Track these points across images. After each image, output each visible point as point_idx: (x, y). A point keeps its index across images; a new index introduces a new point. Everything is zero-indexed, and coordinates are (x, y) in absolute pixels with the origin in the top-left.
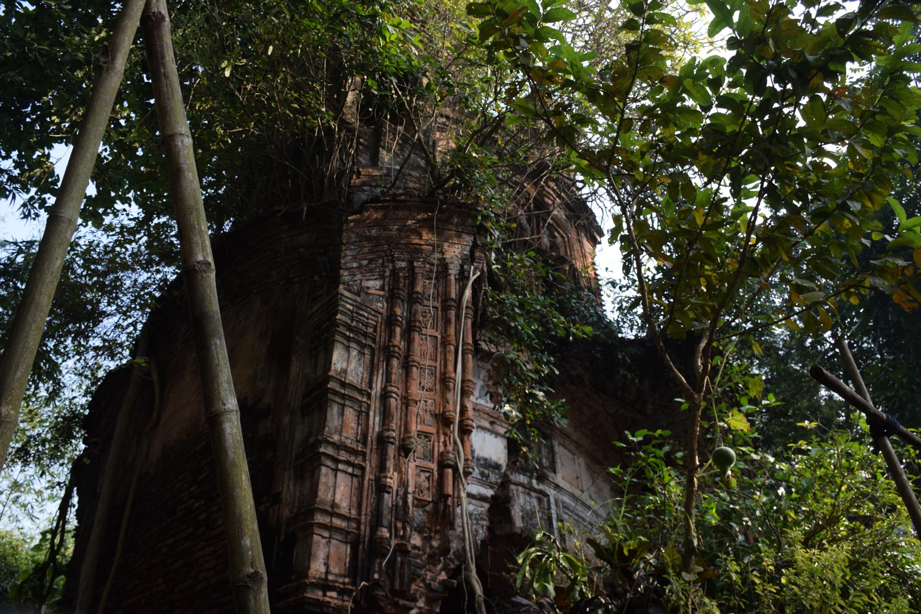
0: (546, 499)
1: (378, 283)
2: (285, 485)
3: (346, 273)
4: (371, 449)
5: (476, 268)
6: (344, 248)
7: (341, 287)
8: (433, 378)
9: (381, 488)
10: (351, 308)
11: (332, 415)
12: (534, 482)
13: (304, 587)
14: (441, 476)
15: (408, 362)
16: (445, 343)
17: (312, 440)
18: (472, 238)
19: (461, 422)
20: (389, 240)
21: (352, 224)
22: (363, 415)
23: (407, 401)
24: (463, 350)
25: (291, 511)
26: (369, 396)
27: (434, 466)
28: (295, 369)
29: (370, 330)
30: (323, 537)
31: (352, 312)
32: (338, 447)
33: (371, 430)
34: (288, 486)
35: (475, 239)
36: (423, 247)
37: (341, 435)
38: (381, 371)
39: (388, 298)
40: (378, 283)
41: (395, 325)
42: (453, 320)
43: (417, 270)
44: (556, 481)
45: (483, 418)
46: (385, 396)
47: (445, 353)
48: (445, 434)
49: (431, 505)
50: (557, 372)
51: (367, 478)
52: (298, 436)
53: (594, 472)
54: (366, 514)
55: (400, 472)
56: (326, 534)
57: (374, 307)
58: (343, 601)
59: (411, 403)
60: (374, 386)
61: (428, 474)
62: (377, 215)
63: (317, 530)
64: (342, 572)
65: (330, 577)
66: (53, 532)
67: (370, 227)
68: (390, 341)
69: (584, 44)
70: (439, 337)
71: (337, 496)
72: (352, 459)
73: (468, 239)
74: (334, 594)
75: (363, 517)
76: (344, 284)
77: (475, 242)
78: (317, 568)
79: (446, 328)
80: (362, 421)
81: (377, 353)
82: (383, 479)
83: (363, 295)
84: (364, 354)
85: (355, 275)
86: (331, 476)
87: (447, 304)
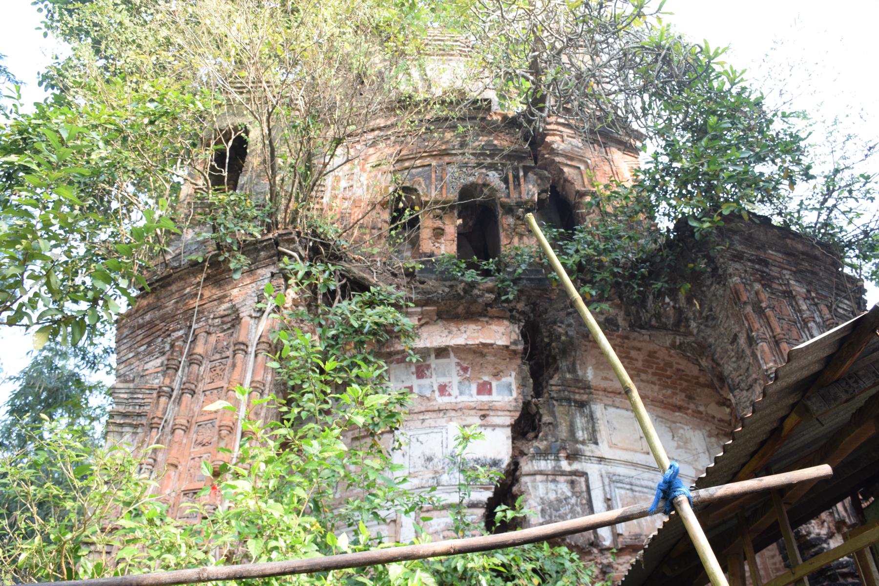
0: (583, 479)
10: (126, 396)
45: (469, 415)
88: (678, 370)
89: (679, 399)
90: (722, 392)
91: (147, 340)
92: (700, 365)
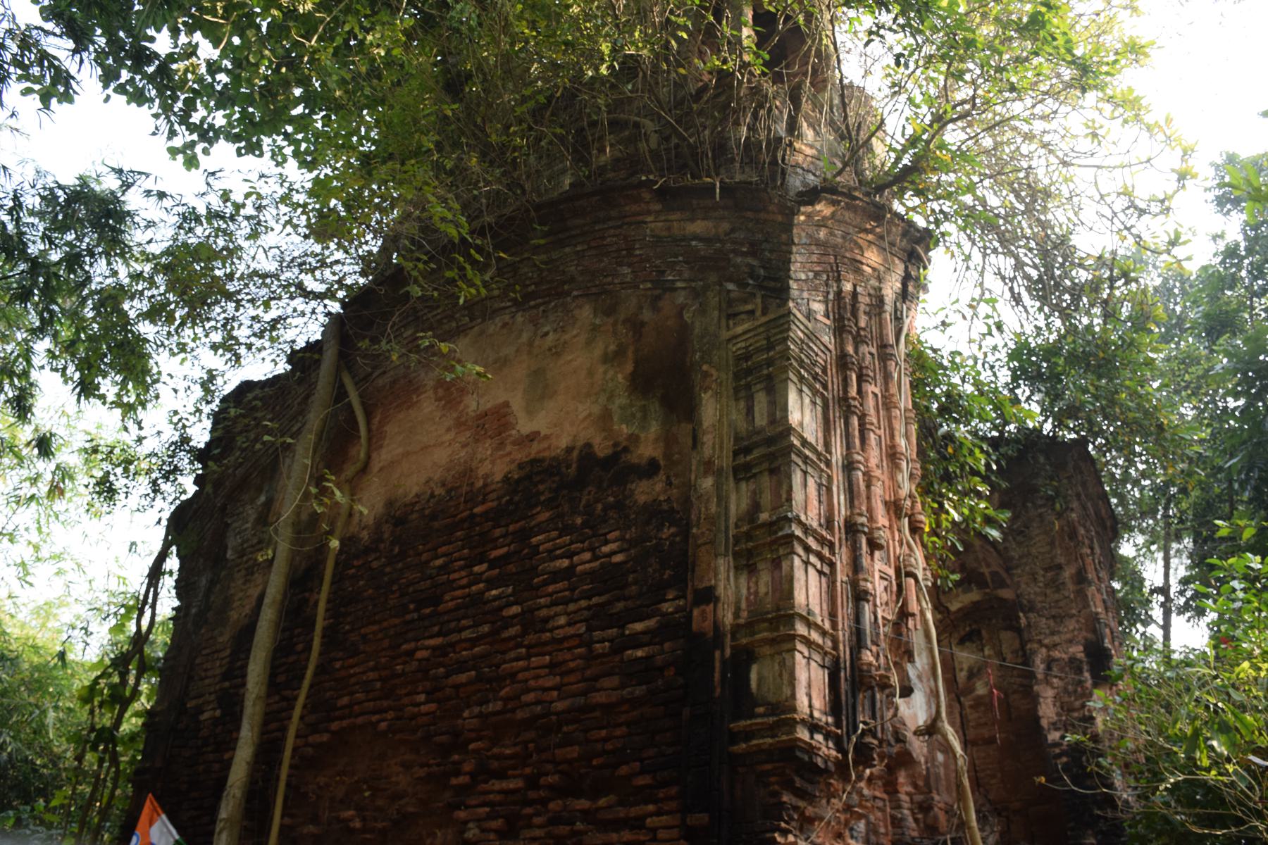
2: (722, 576)
4: (840, 539)
6: (794, 249)
13: (793, 723)
17: (764, 516)
21: (802, 218)
22: (825, 489)
25: (736, 615)
26: (828, 464)
28: (709, 410)
31: (803, 342)
35: (906, 268)
36: (865, 268)
38: (838, 432)
41: (851, 369)
46: (849, 467)
61: (886, 583)
80: (824, 498)
82: (862, 583)
91: (818, 269)
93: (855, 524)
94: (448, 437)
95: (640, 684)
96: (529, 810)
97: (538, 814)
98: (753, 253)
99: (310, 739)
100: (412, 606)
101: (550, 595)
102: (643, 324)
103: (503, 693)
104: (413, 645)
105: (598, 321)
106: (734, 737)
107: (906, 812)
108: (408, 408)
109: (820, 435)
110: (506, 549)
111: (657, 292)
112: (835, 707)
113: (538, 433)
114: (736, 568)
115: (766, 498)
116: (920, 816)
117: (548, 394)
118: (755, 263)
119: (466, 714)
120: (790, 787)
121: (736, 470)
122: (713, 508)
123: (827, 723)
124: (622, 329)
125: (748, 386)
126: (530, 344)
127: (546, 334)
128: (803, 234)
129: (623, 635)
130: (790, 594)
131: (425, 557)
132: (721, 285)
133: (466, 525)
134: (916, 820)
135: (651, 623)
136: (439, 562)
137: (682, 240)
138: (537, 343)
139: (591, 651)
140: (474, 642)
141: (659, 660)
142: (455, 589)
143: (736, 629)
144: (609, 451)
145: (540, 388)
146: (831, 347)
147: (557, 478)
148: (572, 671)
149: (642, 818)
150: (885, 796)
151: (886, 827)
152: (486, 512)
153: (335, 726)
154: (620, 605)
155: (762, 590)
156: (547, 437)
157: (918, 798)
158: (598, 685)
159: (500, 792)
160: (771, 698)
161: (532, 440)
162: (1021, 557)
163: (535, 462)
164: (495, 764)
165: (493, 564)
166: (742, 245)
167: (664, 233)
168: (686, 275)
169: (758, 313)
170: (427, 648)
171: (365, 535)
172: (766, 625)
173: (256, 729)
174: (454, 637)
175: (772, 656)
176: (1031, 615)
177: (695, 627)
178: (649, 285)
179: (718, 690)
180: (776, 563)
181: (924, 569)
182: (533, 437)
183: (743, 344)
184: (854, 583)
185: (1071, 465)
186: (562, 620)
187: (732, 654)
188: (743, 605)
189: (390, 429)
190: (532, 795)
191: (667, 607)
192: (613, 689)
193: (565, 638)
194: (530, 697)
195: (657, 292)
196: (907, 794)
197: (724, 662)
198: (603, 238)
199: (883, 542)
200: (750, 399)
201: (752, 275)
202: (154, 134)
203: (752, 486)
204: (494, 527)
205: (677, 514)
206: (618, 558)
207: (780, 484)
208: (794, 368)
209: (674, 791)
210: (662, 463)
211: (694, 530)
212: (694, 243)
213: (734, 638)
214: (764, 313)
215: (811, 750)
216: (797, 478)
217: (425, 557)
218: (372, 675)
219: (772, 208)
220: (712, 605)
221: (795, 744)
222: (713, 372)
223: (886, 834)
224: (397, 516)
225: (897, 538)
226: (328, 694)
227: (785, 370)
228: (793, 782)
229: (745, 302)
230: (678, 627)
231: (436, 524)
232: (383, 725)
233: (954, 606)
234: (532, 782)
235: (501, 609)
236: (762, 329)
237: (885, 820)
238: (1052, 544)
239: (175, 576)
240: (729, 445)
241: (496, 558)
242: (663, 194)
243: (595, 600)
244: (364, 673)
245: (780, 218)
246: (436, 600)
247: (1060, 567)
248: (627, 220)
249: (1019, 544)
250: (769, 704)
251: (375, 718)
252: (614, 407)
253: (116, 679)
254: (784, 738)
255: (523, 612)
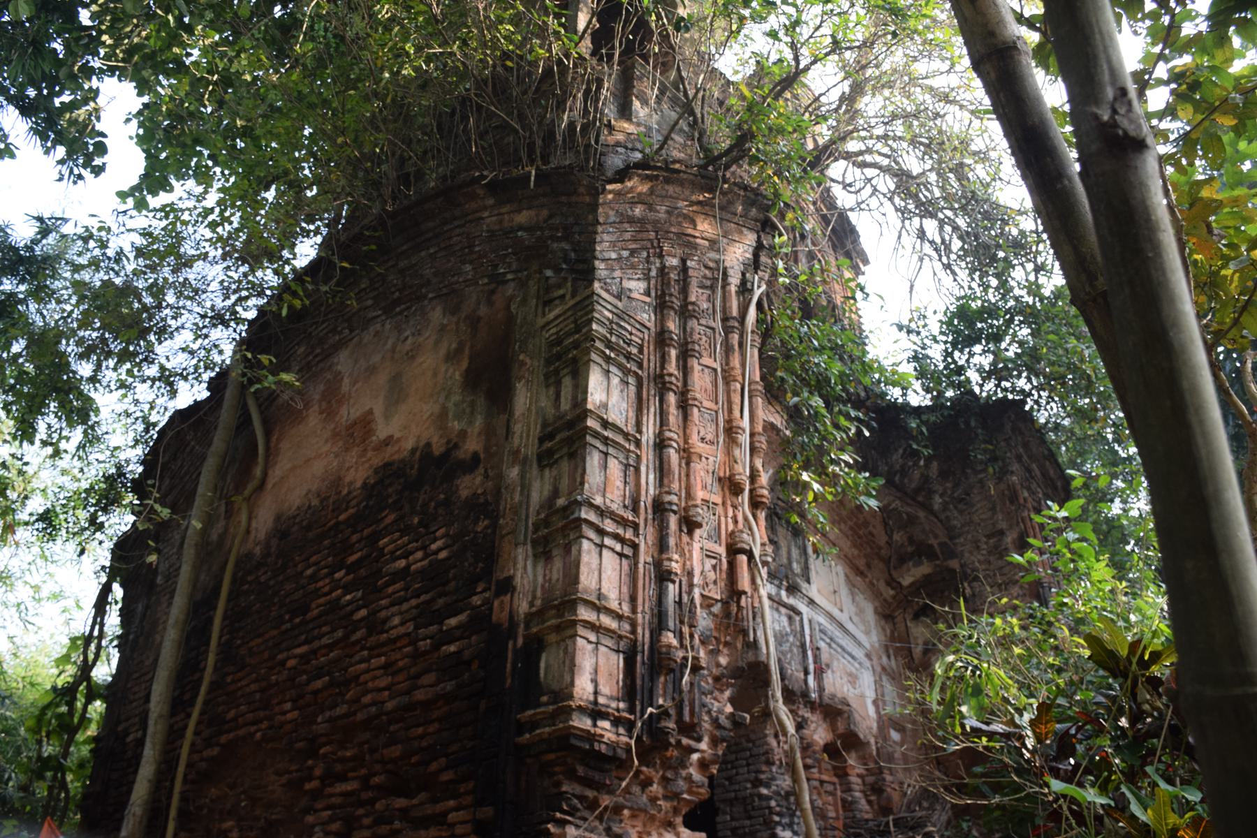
0: (798, 618)
1: (642, 286)
2: (520, 566)
3: (602, 266)
4: (646, 520)
5: (761, 279)
6: (600, 229)
7: (596, 285)
8: (714, 427)
9: (663, 576)
10: (610, 316)
11: (592, 467)
12: (783, 593)
13: (568, 711)
14: (732, 565)
15: (687, 400)
16: (728, 380)
17: (561, 502)
18: (755, 236)
19: (751, 491)
20: (657, 226)
21: (610, 196)
22: (632, 469)
23: (687, 455)
24: (750, 391)
25: (531, 604)
26: (638, 443)
27: (722, 550)
28: (522, 400)
29: (635, 351)
30: (590, 642)
31: (611, 322)
32: (602, 512)
33: (643, 493)
34: (525, 567)
35: (759, 237)
36: (698, 241)
37: (604, 496)
38: (652, 410)
39: (655, 308)
40: (642, 286)
41: (669, 346)
42: (736, 347)
43: (691, 272)
44: (810, 595)
46: (661, 445)
47: (728, 393)
48: (735, 507)
49: (719, 605)
50: (867, 434)
51: (642, 560)
52: (536, 498)
53: (854, 586)
54: (643, 611)
55: (682, 554)
56: (593, 638)
57: (638, 318)
58: (618, 735)
59: (694, 458)
60: (644, 430)
61: (714, 561)
62: (644, 188)
63: (581, 631)
64: (615, 694)
65: (601, 700)
66: (88, 639)
67: (633, 203)
68: (663, 367)
69: (188, 249)
70: (719, 370)
71: (603, 583)
72: (620, 531)
73: (750, 238)
74: (606, 724)
75: (640, 616)
76: (600, 280)
77: (759, 241)
78: (583, 687)
79: (727, 357)
80: (631, 479)
81: (645, 383)
82: (666, 563)
83: (625, 299)
84: (627, 383)
85: (613, 270)
86: (595, 550)
87: (732, 324)
88: (871, 533)
89: (861, 563)
90: (893, 572)
91: (634, 246)
92: (891, 537)
93: (663, 503)
94: (325, 449)
95: (450, 680)
96: (361, 811)
97: (366, 816)
98: (565, 238)
99: (205, 754)
100: (287, 617)
101: (390, 596)
102: (479, 319)
103: (348, 697)
104: (285, 655)
105: (445, 322)
106: (521, 728)
107: (857, 794)
108: (300, 423)
109: (632, 414)
110: (359, 554)
111: (493, 286)
112: (630, 692)
113: (391, 437)
114: (535, 556)
115: (565, 483)
116: (873, 798)
117: (400, 398)
118: (567, 247)
119: (319, 719)
120: (572, 776)
121: (540, 458)
122: (517, 497)
123: (618, 710)
124: (463, 327)
125: (557, 372)
126: (393, 350)
127: (407, 338)
128: (612, 213)
129: (441, 631)
130: (576, 580)
131: (300, 567)
132: (541, 273)
133: (332, 533)
134: (869, 802)
135: (462, 617)
136: (309, 572)
137: (510, 232)
138: (398, 348)
139: (416, 649)
140: (330, 647)
141: (467, 654)
142: (319, 597)
143: (530, 617)
144: (442, 449)
145: (396, 393)
146: (651, 325)
147: (402, 480)
148: (401, 670)
149: (445, 814)
150: (835, 780)
151: (837, 811)
152: (348, 519)
153: (223, 739)
154: (441, 601)
155: (555, 576)
156: (399, 440)
157: (870, 779)
158: (420, 682)
159: (342, 794)
160: (555, 686)
161: (387, 445)
162: (963, 526)
163: (387, 465)
164: (339, 767)
165: (351, 569)
166: (557, 230)
167: (497, 227)
168: (514, 267)
169: (568, 297)
170: (295, 657)
171: (258, 550)
172: (553, 612)
173: (158, 747)
174: (316, 644)
175: (558, 643)
176: (975, 584)
177: (494, 618)
178: (486, 280)
179: (509, 681)
180: (567, 549)
181: (763, 545)
182: (388, 441)
183: (554, 331)
184: (658, 564)
185: (1008, 427)
186: (396, 621)
187: (524, 643)
188: (539, 593)
189: (284, 445)
190: (365, 795)
191: (476, 600)
192: (431, 686)
193: (399, 638)
194: (367, 699)
195: (493, 286)
196: (859, 776)
197: (515, 651)
198: (450, 238)
199: (699, 519)
200: (559, 383)
201: (566, 259)
202: (60, 180)
203: (555, 472)
204: (353, 533)
205: (486, 507)
206: (443, 555)
207: (576, 468)
208: (597, 349)
209: (471, 785)
210: (482, 456)
211: (501, 521)
212: (520, 234)
213: (527, 626)
214: (573, 296)
215: (591, 737)
216: (593, 460)
217: (300, 567)
218: (253, 687)
219: (581, 190)
220: (509, 596)
221: (570, 733)
222: (528, 361)
223: (837, 818)
224: (282, 530)
225: (730, 514)
226: (221, 708)
227: (587, 352)
228: (575, 771)
229: (559, 286)
230: (481, 620)
231: (310, 535)
232: (259, 734)
233: (906, 581)
234: (365, 780)
235: (352, 613)
236: (570, 313)
237: (835, 805)
238: (993, 509)
239: (120, 605)
240: (536, 431)
241: (353, 563)
242: (493, 187)
243: (423, 598)
244: (248, 685)
245: (587, 199)
246: (305, 609)
247: (1002, 533)
248: (469, 217)
249: (961, 512)
250: (553, 692)
251: (253, 729)
252: (450, 405)
253: (64, 709)
254: (561, 725)
255: (369, 615)
